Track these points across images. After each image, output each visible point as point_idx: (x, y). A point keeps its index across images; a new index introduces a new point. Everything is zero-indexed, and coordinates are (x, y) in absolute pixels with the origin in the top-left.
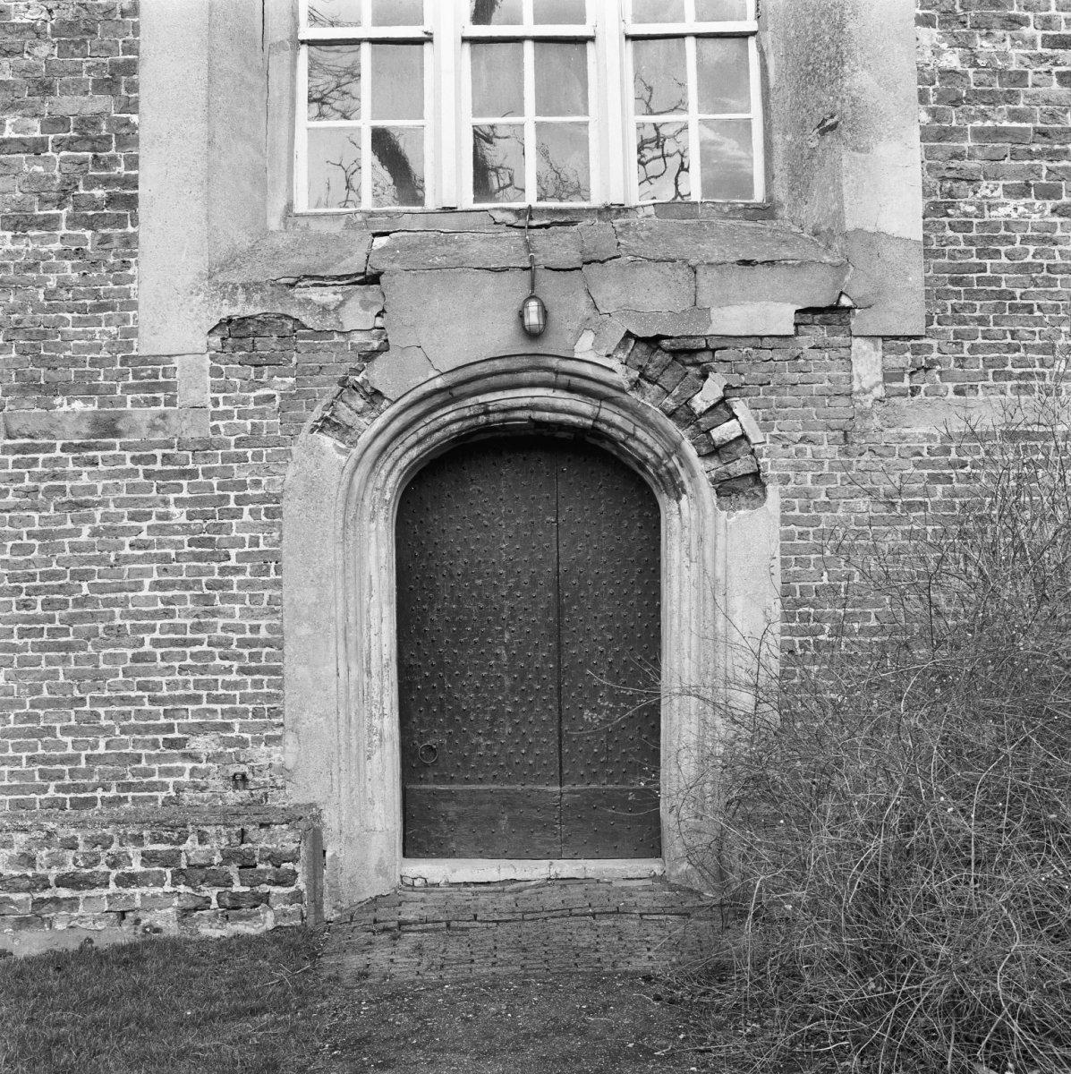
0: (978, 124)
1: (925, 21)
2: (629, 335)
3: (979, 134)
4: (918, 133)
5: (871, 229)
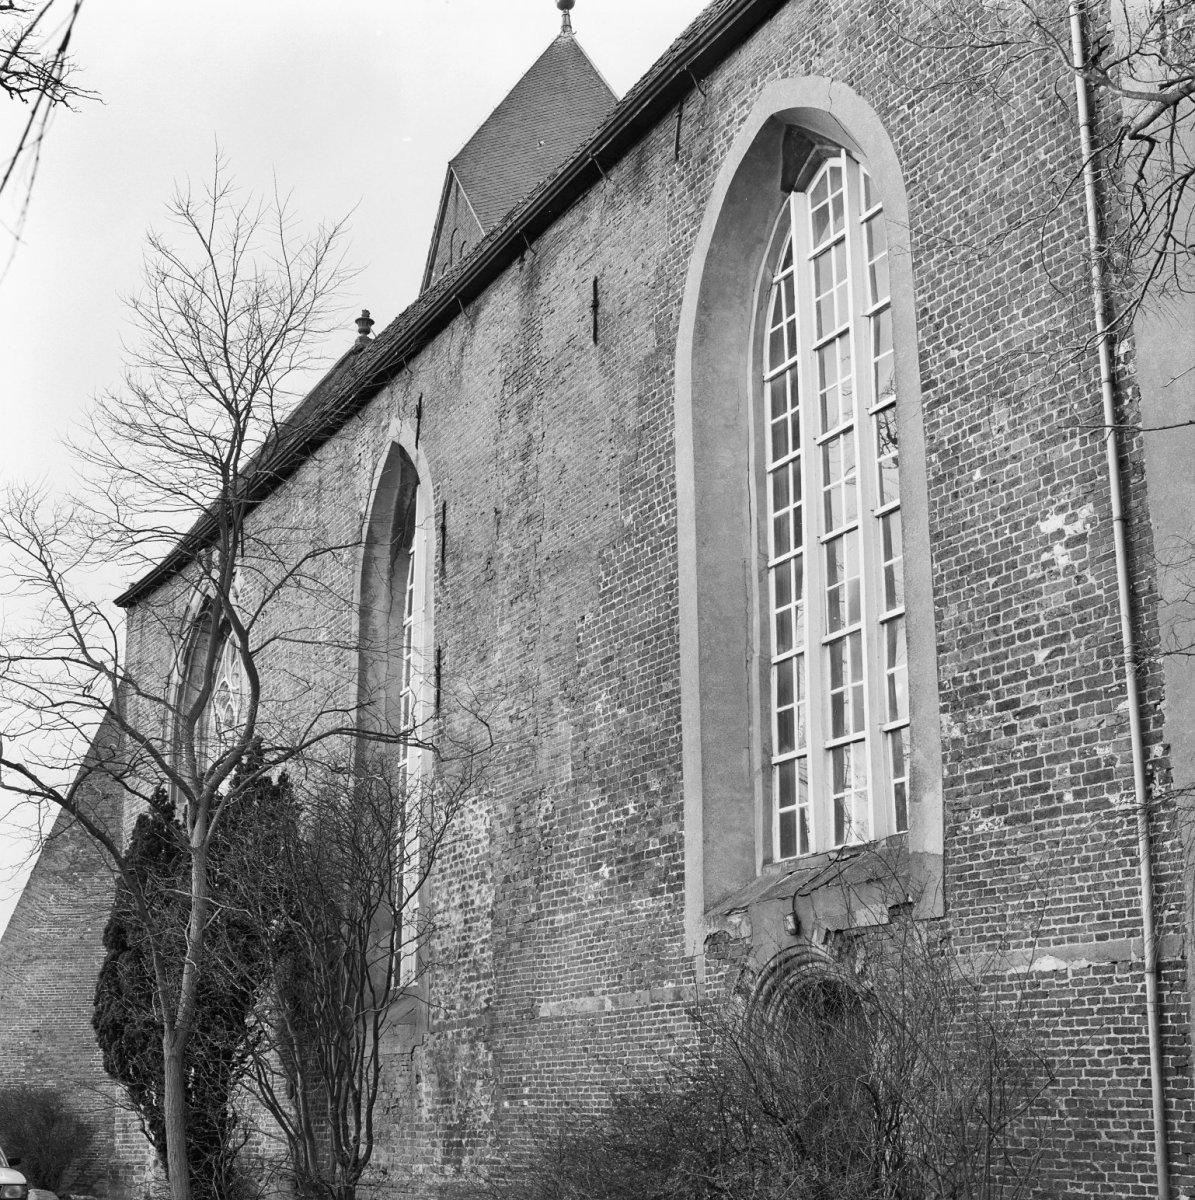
0: (969, 771)
1: (944, 710)
2: (828, 932)
3: (972, 778)
4: (940, 782)
5: (920, 851)
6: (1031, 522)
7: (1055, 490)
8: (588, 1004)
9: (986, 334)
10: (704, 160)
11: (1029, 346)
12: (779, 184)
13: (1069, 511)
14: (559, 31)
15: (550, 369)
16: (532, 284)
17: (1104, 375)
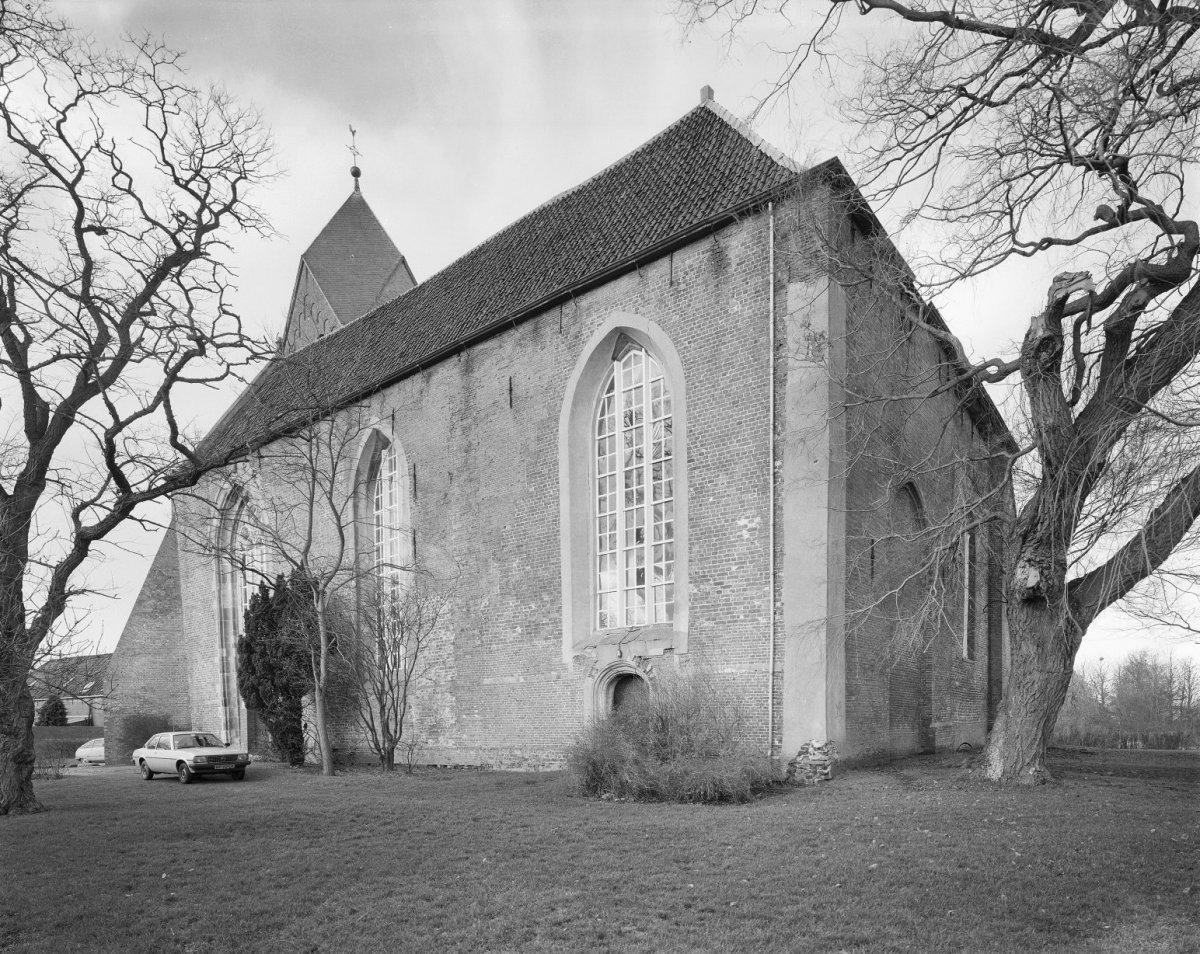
1: (691, 582)
6: (733, 520)
7: (745, 510)
8: (511, 680)
9: (719, 445)
10: (577, 337)
11: (738, 455)
12: (611, 357)
13: (751, 519)
14: (353, 190)
15: (483, 414)
16: (468, 369)
17: (771, 473)
